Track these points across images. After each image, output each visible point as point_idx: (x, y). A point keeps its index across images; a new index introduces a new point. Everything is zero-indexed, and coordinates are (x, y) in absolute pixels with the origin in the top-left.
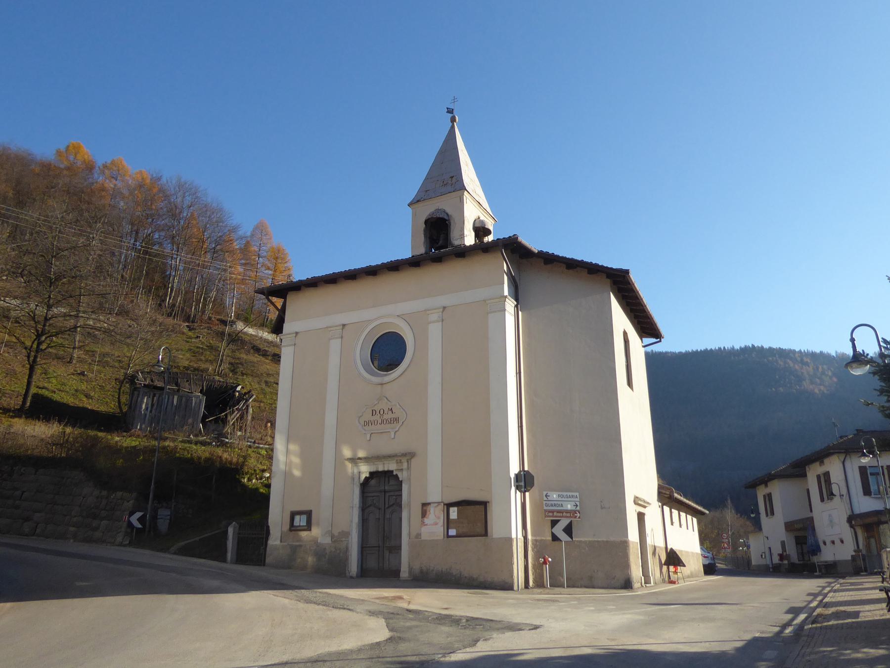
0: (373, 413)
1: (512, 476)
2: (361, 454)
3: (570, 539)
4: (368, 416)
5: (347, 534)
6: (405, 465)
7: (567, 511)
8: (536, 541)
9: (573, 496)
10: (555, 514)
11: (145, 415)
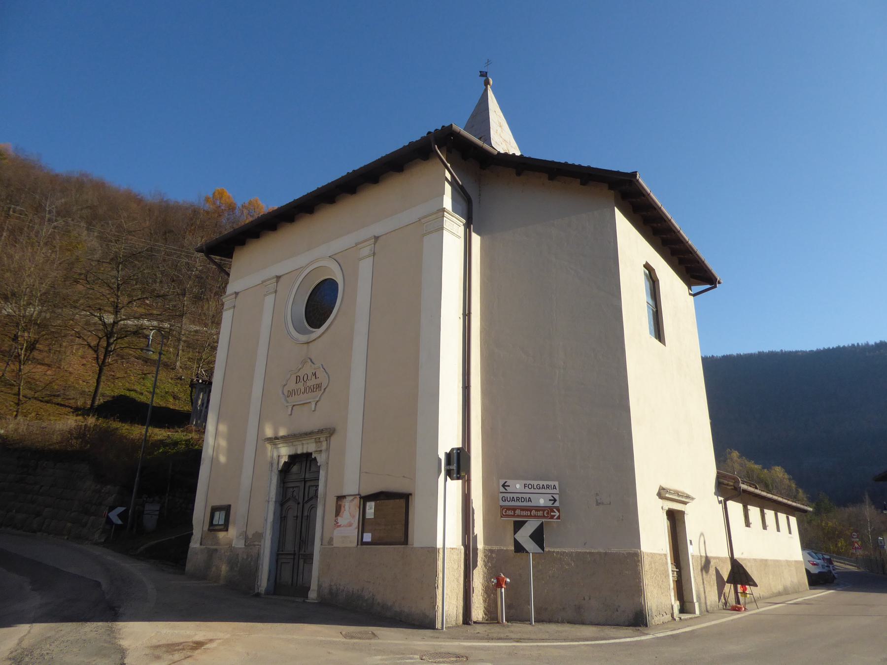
0: (298, 379)
1: (442, 456)
2: (282, 432)
3: (541, 551)
4: (292, 385)
5: (259, 536)
6: (324, 444)
7: (538, 509)
8: (491, 551)
9: (548, 487)
10: (518, 512)
11: (201, 411)
